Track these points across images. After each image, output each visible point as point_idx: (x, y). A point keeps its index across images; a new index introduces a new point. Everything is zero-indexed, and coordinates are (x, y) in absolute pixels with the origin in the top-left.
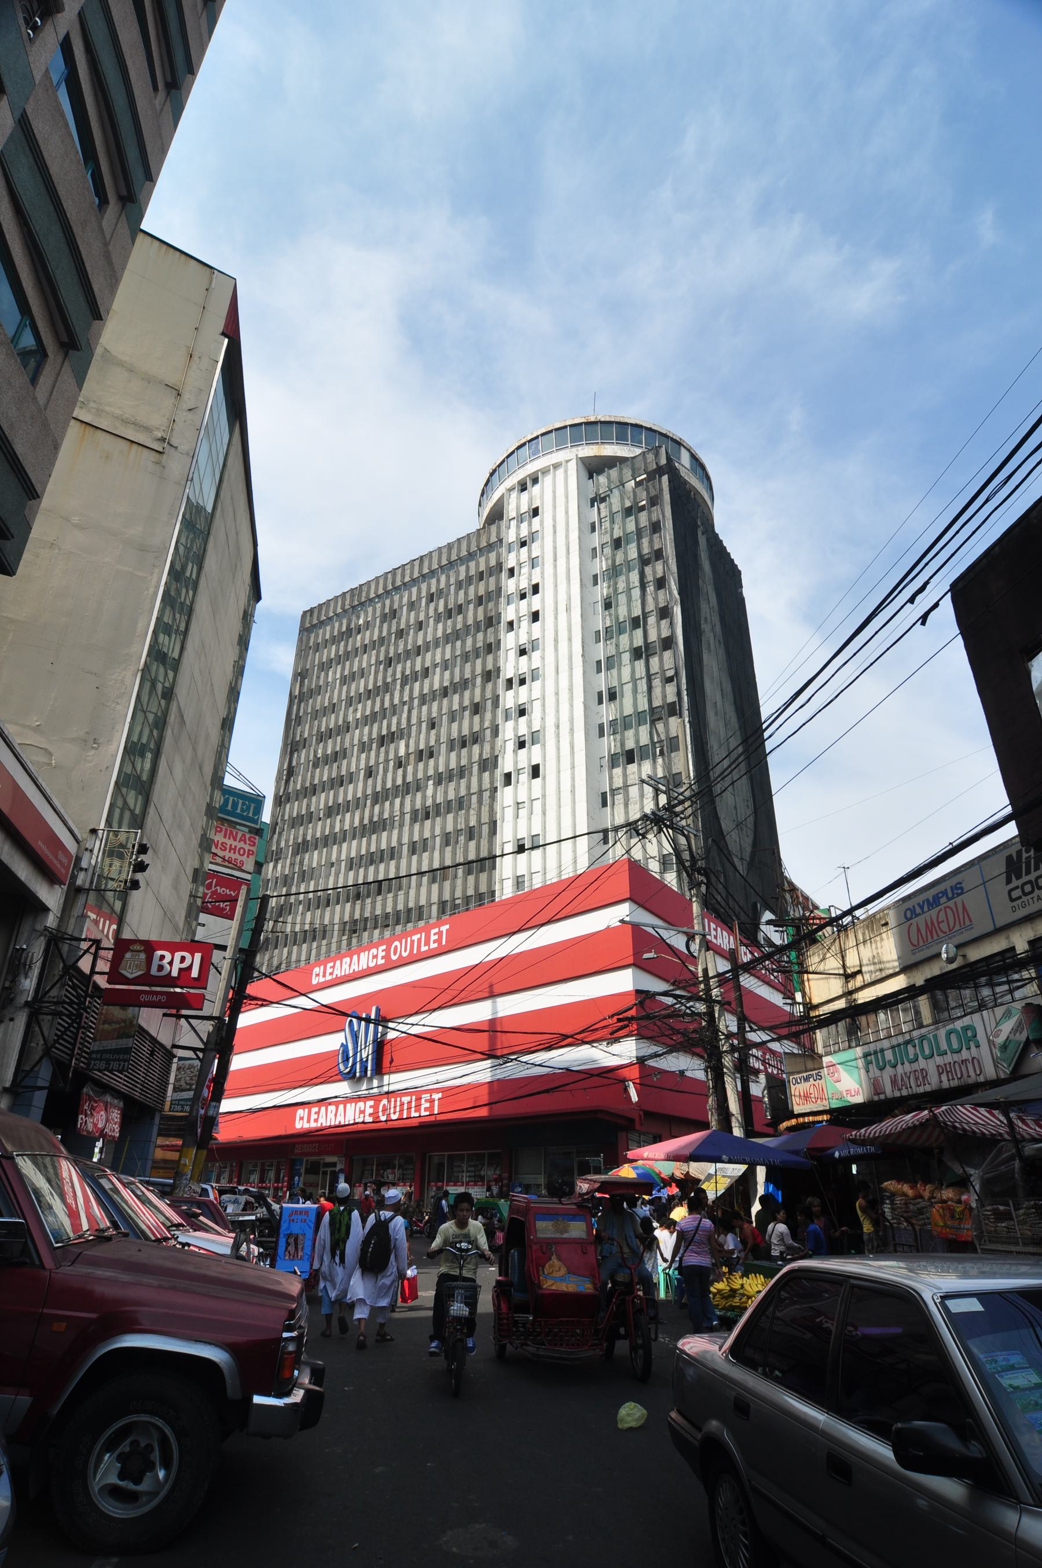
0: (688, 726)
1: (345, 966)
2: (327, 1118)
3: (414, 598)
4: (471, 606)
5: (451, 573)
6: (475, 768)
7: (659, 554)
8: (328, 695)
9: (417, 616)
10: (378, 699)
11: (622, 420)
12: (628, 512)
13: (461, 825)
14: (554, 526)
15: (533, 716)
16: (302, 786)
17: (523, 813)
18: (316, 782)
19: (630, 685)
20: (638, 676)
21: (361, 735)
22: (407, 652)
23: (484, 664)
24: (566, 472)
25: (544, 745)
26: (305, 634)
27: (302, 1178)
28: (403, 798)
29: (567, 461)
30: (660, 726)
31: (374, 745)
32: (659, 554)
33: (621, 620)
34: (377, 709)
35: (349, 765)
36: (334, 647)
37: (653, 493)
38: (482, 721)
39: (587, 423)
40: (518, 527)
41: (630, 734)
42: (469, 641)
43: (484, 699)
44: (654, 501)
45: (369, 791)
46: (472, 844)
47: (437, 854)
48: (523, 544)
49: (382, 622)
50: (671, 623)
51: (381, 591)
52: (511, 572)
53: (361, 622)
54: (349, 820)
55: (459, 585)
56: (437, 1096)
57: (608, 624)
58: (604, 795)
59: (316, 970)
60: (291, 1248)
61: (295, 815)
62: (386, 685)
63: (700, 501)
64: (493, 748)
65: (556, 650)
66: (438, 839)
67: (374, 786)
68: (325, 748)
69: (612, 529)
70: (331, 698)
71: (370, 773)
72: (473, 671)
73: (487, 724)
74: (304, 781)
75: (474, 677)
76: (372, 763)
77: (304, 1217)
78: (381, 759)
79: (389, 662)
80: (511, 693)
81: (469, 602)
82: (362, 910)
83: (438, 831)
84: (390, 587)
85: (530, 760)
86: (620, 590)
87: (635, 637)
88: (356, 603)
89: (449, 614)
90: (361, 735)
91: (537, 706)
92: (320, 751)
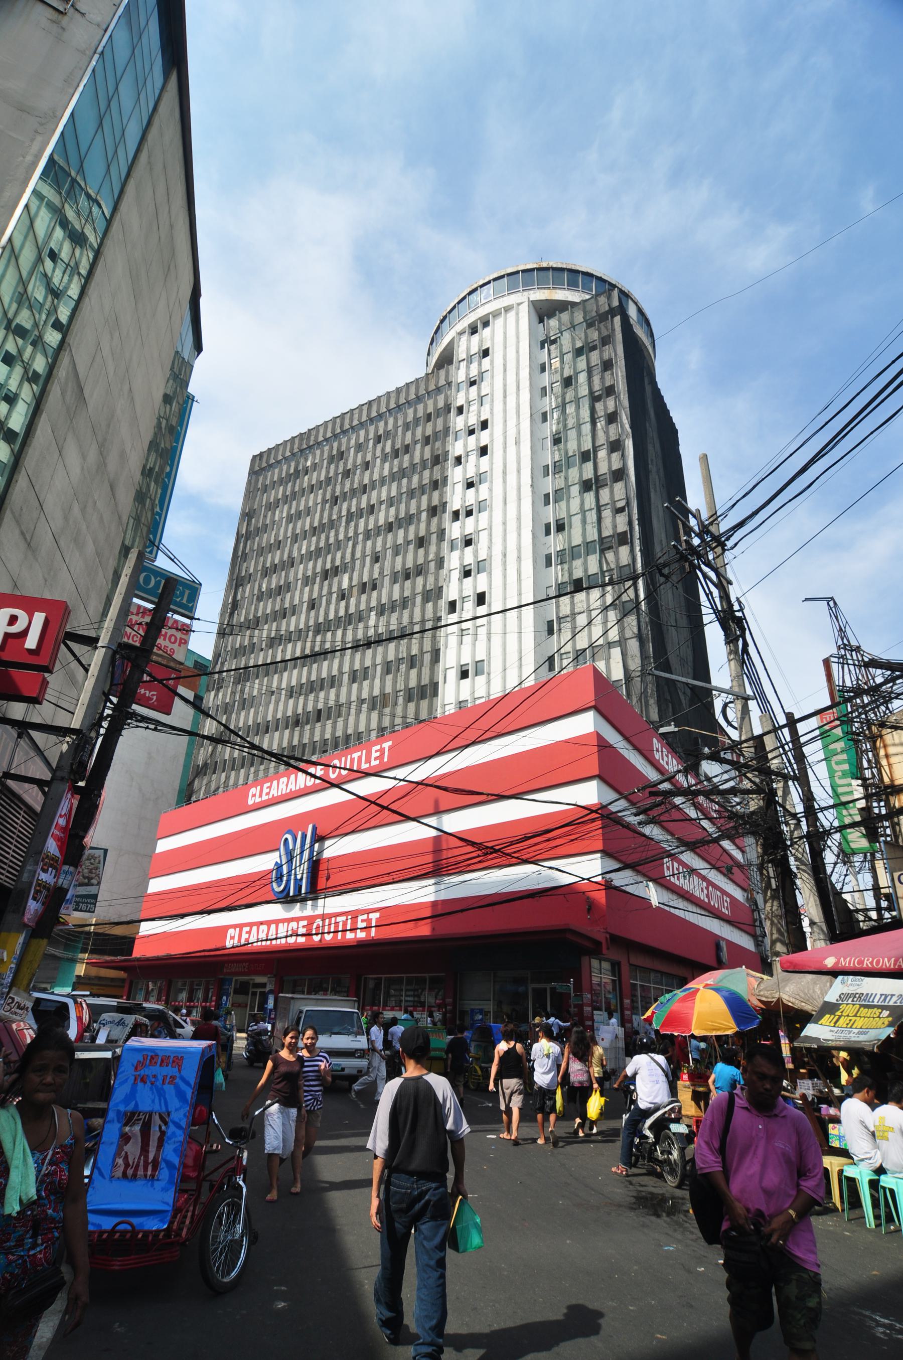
0: (639, 555)
1: (282, 786)
2: (257, 938)
3: (362, 440)
4: (418, 446)
5: (399, 416)
6: (419, 599)
7: (610, 391)
8: (274, 533)
9: (364, 456)
10: (323, 536)
11: (573, 267)
12: (579, 352)
13: (403, 654)
14: (505, 365)
15: (480, 546)
16: (245, 618)
17: (467, 639)
18: (260, 614)
19: (579, 516)
20: (587, 507)
21: (305, 569)
22: (353, 491)
23: (430, 500)
24: (517, 314)
25: (490, 574)
26: (254, 477)
27: (230, 998)
28: (345, 630)
29: (519, 304)
30: (610, 556)
31: (318, 579)
32: (610, 391)
33: (570, 454)
34: (322, 544)
35: (292, 598)
36: (281, 488)
37: (605, 333)
38: (426, 554)
39: (540, 269)
40: (468, 367)
41: (578, 563)
42: (415, 478)
43: (429, 533)
44: (606, 341)
45: (311, 623)
46: (414, 673)
47: (377, 682)
48: (473, 383)
49: (329, 463)
50: (623, 455)
51: (329, 435)
52: (460, 410)
53: (309, 463)
54: (291, 650)
55: (407, 427)
56: (374, 916)
57: (557, 458)
58: (550, 624)
59: (253, 791)
60: (133, 1149)
61: (238, 646)
62: (331, 521)
63: (646, 354)
64: (437, 579)
65: (505, 481)
66: (379, 668)
67: (317, 617)
68: (269, 583)
69: (562, 369)
70: (277, 535)
71: (312, 605)
72: (419, 507)
73: (431, 556)
74: (247, 614)
75: (419, 512)
76: (315, 595)
77: (170, 1071)
78: (325, 592)
79: (335, 500)
80: (457, 524)
81: (416, 442)
82: (301, 736)
83: (379, 660)
84: (338, 431)
85: (475, 588)
86: (570, 426)
87: (584, 470)
88: (305, 446)
89: (396, 453)
90: (305, 569)
91: (483, 536)
92: (264, 586)
